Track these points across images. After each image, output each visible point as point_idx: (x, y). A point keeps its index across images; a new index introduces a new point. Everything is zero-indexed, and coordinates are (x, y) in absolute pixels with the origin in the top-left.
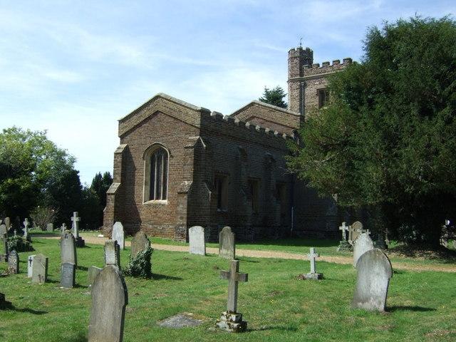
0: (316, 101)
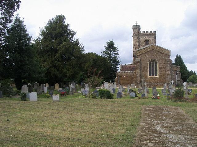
0: (144, 43)
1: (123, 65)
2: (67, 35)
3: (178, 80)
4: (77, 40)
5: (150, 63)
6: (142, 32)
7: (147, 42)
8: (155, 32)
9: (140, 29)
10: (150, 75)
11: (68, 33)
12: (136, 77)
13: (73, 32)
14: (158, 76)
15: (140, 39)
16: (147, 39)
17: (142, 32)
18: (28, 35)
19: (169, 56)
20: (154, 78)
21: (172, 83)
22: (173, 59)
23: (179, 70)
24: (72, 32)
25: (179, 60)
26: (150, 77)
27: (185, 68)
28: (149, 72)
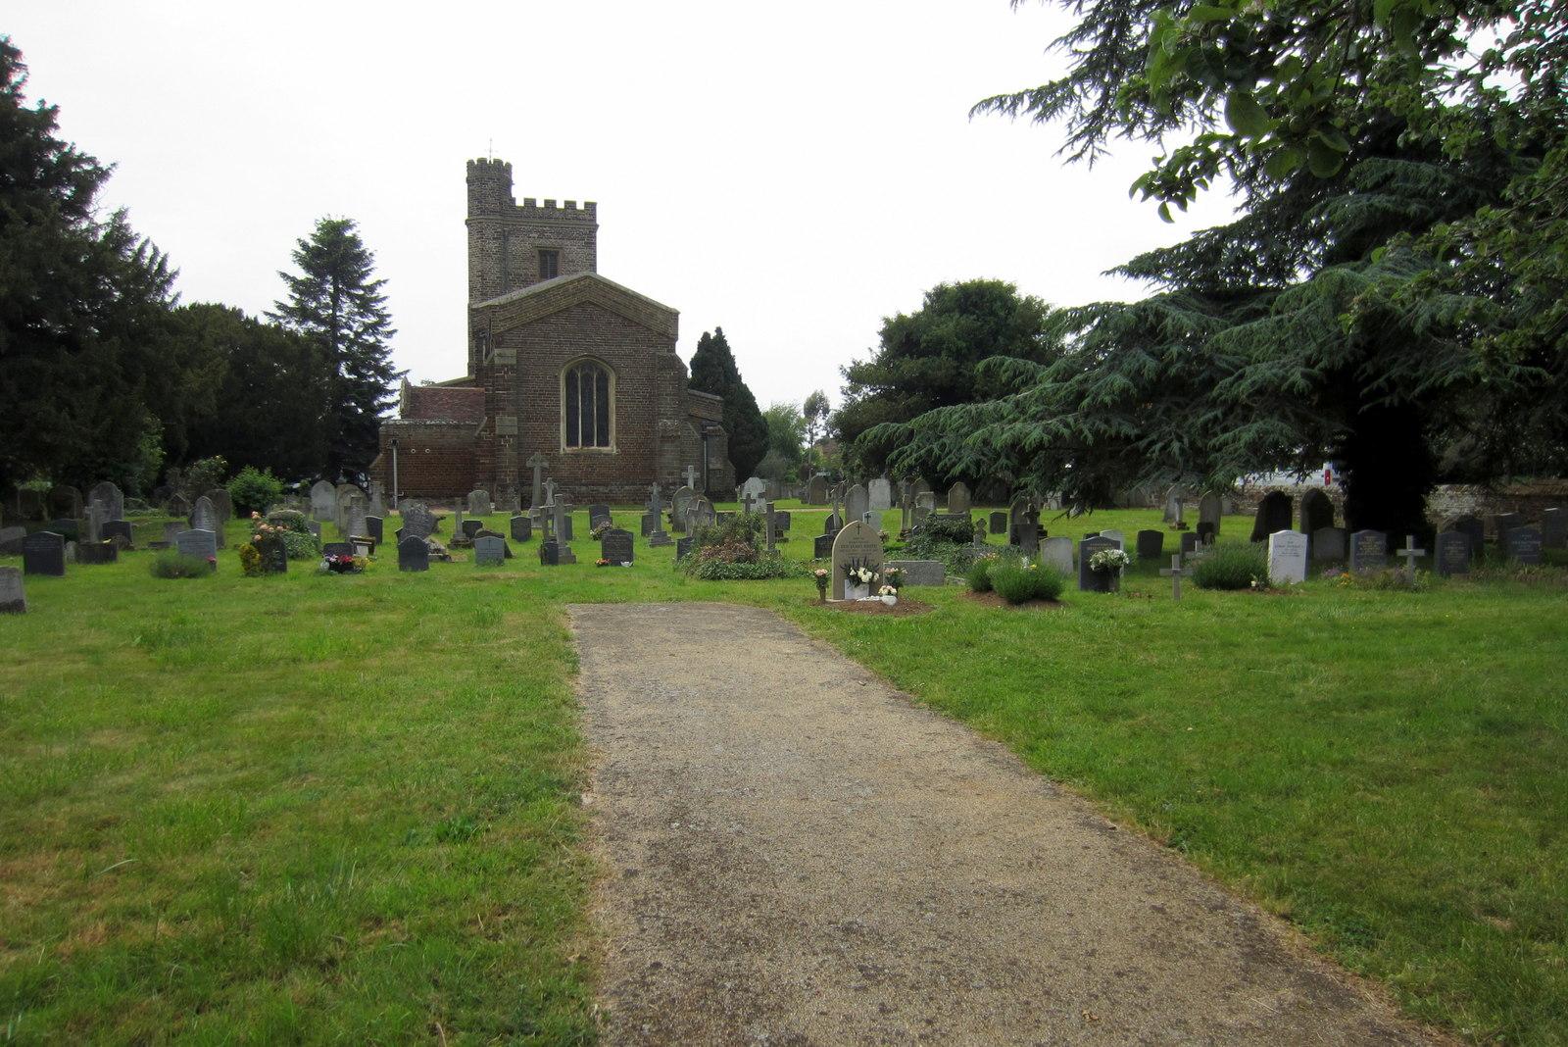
0: (534, 268)
1: (415, 381)
2: (46, 183)
3: (711, 467)
4: (120, 215)
5: (571, 379)
6: (520, 203)
7: (549, 260)
8: (591, 207)
9: (509, 184)
10: (572, 441)
11: (48, 166)
12: (494, 449)
13: (87, 167)
14: (612, 449)
15: (512, 239)
16: (549, 242)
17: (520, 203)
18: (570, 205)
19: (672, 338)
20: (591, 456)
21: (691, 484)
22: (686, 349)
23: (720, 417)
24: (81, 159)
25: (714, 350)
26: (569, 450)
27: (746, 399)
28: (563, 426)
